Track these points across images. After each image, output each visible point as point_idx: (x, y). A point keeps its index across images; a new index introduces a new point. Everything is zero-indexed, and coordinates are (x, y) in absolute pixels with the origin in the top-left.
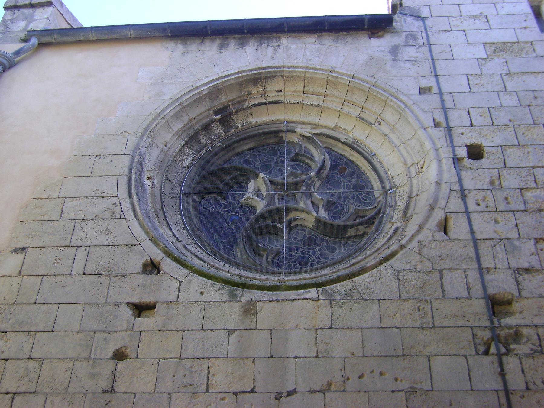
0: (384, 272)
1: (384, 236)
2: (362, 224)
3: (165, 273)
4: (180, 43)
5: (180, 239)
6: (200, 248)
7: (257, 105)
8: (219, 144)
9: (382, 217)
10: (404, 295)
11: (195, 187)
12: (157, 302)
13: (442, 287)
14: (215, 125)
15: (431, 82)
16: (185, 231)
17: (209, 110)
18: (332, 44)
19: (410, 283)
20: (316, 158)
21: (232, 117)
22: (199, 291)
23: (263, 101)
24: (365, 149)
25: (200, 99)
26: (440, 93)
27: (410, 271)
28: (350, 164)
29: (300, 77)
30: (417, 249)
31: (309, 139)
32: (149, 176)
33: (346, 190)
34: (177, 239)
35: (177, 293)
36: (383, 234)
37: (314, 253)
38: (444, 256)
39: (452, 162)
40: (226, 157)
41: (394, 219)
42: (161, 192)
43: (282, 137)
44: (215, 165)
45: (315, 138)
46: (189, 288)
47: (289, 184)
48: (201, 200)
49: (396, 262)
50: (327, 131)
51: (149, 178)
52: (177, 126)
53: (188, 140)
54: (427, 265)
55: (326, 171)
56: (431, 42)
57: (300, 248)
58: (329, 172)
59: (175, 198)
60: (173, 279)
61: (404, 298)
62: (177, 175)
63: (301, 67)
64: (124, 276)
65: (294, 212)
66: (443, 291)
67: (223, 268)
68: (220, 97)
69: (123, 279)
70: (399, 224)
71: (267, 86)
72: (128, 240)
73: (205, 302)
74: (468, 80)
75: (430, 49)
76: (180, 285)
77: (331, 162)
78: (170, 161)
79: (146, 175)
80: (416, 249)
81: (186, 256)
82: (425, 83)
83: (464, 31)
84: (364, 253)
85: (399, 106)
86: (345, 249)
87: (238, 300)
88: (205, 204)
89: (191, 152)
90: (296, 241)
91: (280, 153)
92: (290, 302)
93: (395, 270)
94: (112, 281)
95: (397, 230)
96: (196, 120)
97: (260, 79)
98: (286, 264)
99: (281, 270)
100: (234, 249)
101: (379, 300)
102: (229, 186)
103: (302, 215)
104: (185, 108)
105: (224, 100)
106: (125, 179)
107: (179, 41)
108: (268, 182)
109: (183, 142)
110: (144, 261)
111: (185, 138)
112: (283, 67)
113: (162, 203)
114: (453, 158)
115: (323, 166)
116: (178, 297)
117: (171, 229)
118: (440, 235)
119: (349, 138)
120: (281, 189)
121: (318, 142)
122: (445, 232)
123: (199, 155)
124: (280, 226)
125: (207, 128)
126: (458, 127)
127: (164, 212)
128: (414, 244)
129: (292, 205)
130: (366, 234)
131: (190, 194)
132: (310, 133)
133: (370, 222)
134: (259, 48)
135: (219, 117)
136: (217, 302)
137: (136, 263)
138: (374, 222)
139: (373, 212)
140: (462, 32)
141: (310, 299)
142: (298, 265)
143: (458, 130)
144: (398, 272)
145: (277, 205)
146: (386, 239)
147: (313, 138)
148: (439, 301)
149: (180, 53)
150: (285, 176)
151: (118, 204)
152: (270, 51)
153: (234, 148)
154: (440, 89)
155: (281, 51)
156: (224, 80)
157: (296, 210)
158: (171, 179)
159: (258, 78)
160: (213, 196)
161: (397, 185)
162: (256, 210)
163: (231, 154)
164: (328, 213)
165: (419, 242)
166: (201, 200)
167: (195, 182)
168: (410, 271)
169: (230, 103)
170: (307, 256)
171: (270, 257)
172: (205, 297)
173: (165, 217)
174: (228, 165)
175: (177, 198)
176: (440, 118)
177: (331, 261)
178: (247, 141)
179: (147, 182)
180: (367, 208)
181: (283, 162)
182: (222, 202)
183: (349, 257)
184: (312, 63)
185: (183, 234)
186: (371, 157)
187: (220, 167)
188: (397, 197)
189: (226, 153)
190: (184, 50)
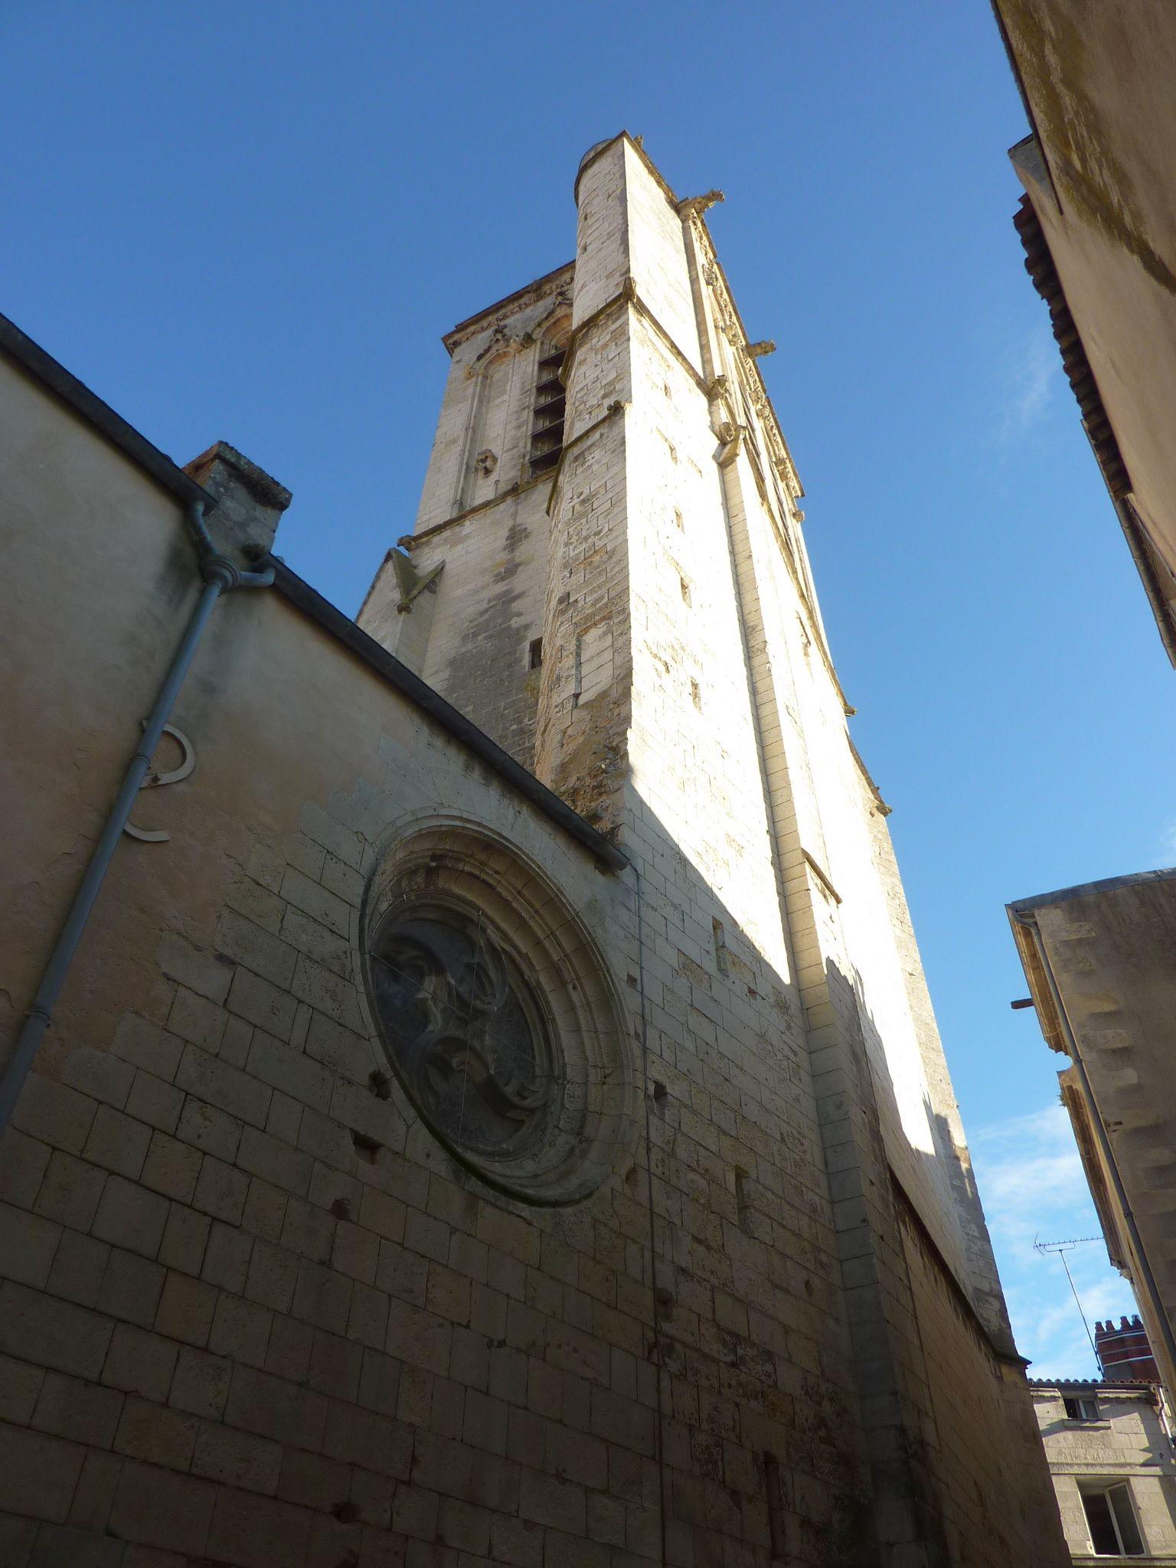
7: (471, 874)
159: (491, 846)
161: (569, 1077)
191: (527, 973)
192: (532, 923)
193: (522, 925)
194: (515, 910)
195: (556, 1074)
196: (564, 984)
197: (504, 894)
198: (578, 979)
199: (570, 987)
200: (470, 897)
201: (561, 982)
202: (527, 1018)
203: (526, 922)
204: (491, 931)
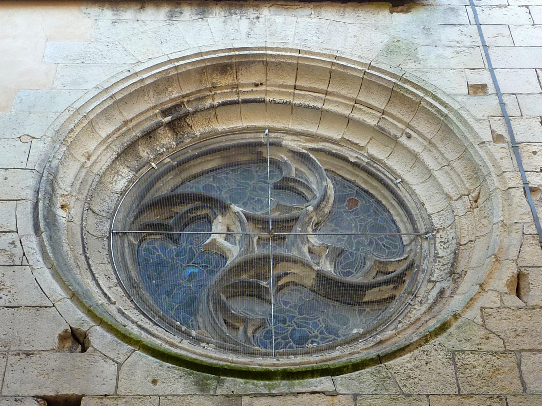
0: (434, 353)
1: (421, 303)
2: (386, 283)
3: (95, 350)
4: (108, 8)
5: (113, 300)
6: (143, 314)
7: (225, 104)
8: (168, 160)
9: (417, 272)
10: (466, 389)
11: (133, 222)
12: (83, 395)
13: (521, 377)
14: (161, 131)
15: (485, 78)
16: (119, 288)
17: (153, 108)
18: (337, 18)
19: (474, 371)
20: (314, 186)
21: (187, 120)
22: (150, 379)
23: (235, 98)
24: (386, 173)
25: (138, 92)
26: (498, 93)
27: (472, 352)
28: (364, 194)
29: (290, 64)
30: (480, 320)
31: (303, 158)
32: (64, 203)
33: (360, 233)
34: (109, 299)
35: (114, 381)
36: (419, 299)
37: (316, 326)
38: (520, 330)
39: (523, 193)
40: (179, 180)
41: (435, 275)
42: (82, 229)
43: (261, 153)
44: (164, 188)
45: (312, 156)
46: (133, 374)
47: (276, 222)
48: (141, 242)
49: (449, 340)
50: (328, 146)
51: (62, 207)
52: (105, 129)
53: (122, 153)
54: (495, 344)
55: (330, 205)
56: (481, 20)
57: (294, 317)
58: (333, 207)
59: (102, 237)
60: (108, 359)
61: (465, 392)
62: (105, 204)
63: (291, 50)
64: (28, 354)
65: (283, 264)
66: (523, 383)
67: (180, 345)
68: (170, 89)
69: (28, 359)
70: (445, 284)
71: (240, 77)
72: (37, 299)
73: (159, 396)
74: (538, 77)
75: (480, 29)
76: (119, 369)
77: (335, 192)
78: (95, 183)
79: (59, 201)
80: (479, 320)
81: (125, 326)
82: (476, 79)
83: (527, 7)
84: (392, 327)
85: (439, 111)
86: (362, 320)
87: (212, 392)
88: (147, 250)
89: (126, 170)
90: (288, 308)
91: (259, 176)
92: (293, 398)
93: (448, 351)
94: (9, 363)
95: (442, 292)
96: (134, 123)
97: (230, 65)
98: (275, 340)
99: (269, 350)
100: (193, 318)
101: (428, 396)
102: (186, 222)
103: (295, 269)
104: (119, 103)
105: (175, 95)
106: (29, 205)
107: (107, 5)
108: (245, 218)
109: (115, 155)
110: (60, 331)
111: (117, 148)
112: (266, 48)
113: (83, 245)
114: (524, 188)
115: (324, 197)
116: (117, 387)
117: (98, 285)
118: (512, 300)
119: (362, 158)
120: (262, 228)
121: (317, 161)
122: (518, 294)
123: (137, 175)
124: (264, 283)
125: (149, 135)
126: (529, 143)
127: (87, 258)
128: (473, 313)
129: (280, 251)
130: (393, 298)
131: (125, 233)
132: (304, 148)
133: (399, 280)
134: (229, 20)
135: (168, 119)
136: (178, 396)
137: (47, 333)
138: (404, 281)
139: (404, 266)
140: (524, 8)
141: (323, 393)
142: (292, 343)
143: (529, 147)
144: (454, 354)
145: (257, 251)
146: (426, 306)
147: (309, 156)
148: (518, 399)
149: (109, 22)
150: (270, 207)
151: (18, 243)
152: (244, 24)
153: (190, 167)
154: (497, 88)
155: (260, 25)
156: (177, 64)
157: (287, 259)
158: (96, 209)
159: (227, 65)
160: (158, 237)
161: (437, 226)
162: (226, 259)
163: (185, 175)
164: (335, 266)
165: (482, 309)
166: (141, 242)
167: (132, 215)
168: (472, 352)
169: (185, 100)
170: (305, 329)
171: (250, 332)
172: (160, 389)
173: (89, 266)
174: (180, 191)
175: (105, 239)
176: (501, 130)
177: (343, 338)
178: (209, 158)
179: (61, 213)
180: (392, 260)
181: (264, 190)
182: (173, 247)
183: (372, 331)
184: (309, 44)
185: (116, 293)
186: (396, 185)
187: (171, 194)
188: (438, 245)
189: (177, 174)
190: (114, 17)
191: (352, 156)
192: (327, 107)
193: (321, 114)
194: (300, 106)
195: (422, 230)
196: (394, 140)
197: (278, 99)
198: (408, 126)
199: (403, 140)
200: (245, 124)
201: (391, 141)
202: (367, 195)
203: (322, 110)
204: (289, 142)
